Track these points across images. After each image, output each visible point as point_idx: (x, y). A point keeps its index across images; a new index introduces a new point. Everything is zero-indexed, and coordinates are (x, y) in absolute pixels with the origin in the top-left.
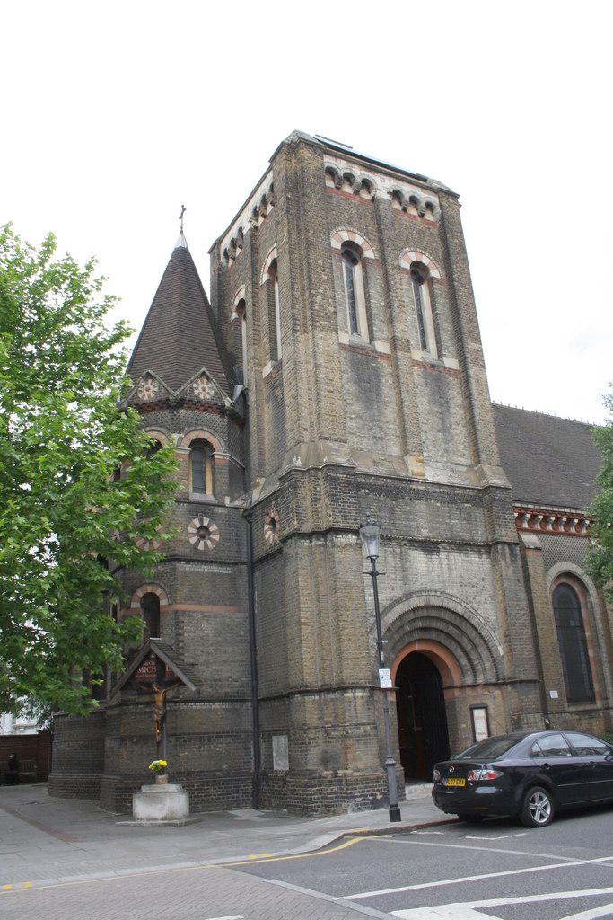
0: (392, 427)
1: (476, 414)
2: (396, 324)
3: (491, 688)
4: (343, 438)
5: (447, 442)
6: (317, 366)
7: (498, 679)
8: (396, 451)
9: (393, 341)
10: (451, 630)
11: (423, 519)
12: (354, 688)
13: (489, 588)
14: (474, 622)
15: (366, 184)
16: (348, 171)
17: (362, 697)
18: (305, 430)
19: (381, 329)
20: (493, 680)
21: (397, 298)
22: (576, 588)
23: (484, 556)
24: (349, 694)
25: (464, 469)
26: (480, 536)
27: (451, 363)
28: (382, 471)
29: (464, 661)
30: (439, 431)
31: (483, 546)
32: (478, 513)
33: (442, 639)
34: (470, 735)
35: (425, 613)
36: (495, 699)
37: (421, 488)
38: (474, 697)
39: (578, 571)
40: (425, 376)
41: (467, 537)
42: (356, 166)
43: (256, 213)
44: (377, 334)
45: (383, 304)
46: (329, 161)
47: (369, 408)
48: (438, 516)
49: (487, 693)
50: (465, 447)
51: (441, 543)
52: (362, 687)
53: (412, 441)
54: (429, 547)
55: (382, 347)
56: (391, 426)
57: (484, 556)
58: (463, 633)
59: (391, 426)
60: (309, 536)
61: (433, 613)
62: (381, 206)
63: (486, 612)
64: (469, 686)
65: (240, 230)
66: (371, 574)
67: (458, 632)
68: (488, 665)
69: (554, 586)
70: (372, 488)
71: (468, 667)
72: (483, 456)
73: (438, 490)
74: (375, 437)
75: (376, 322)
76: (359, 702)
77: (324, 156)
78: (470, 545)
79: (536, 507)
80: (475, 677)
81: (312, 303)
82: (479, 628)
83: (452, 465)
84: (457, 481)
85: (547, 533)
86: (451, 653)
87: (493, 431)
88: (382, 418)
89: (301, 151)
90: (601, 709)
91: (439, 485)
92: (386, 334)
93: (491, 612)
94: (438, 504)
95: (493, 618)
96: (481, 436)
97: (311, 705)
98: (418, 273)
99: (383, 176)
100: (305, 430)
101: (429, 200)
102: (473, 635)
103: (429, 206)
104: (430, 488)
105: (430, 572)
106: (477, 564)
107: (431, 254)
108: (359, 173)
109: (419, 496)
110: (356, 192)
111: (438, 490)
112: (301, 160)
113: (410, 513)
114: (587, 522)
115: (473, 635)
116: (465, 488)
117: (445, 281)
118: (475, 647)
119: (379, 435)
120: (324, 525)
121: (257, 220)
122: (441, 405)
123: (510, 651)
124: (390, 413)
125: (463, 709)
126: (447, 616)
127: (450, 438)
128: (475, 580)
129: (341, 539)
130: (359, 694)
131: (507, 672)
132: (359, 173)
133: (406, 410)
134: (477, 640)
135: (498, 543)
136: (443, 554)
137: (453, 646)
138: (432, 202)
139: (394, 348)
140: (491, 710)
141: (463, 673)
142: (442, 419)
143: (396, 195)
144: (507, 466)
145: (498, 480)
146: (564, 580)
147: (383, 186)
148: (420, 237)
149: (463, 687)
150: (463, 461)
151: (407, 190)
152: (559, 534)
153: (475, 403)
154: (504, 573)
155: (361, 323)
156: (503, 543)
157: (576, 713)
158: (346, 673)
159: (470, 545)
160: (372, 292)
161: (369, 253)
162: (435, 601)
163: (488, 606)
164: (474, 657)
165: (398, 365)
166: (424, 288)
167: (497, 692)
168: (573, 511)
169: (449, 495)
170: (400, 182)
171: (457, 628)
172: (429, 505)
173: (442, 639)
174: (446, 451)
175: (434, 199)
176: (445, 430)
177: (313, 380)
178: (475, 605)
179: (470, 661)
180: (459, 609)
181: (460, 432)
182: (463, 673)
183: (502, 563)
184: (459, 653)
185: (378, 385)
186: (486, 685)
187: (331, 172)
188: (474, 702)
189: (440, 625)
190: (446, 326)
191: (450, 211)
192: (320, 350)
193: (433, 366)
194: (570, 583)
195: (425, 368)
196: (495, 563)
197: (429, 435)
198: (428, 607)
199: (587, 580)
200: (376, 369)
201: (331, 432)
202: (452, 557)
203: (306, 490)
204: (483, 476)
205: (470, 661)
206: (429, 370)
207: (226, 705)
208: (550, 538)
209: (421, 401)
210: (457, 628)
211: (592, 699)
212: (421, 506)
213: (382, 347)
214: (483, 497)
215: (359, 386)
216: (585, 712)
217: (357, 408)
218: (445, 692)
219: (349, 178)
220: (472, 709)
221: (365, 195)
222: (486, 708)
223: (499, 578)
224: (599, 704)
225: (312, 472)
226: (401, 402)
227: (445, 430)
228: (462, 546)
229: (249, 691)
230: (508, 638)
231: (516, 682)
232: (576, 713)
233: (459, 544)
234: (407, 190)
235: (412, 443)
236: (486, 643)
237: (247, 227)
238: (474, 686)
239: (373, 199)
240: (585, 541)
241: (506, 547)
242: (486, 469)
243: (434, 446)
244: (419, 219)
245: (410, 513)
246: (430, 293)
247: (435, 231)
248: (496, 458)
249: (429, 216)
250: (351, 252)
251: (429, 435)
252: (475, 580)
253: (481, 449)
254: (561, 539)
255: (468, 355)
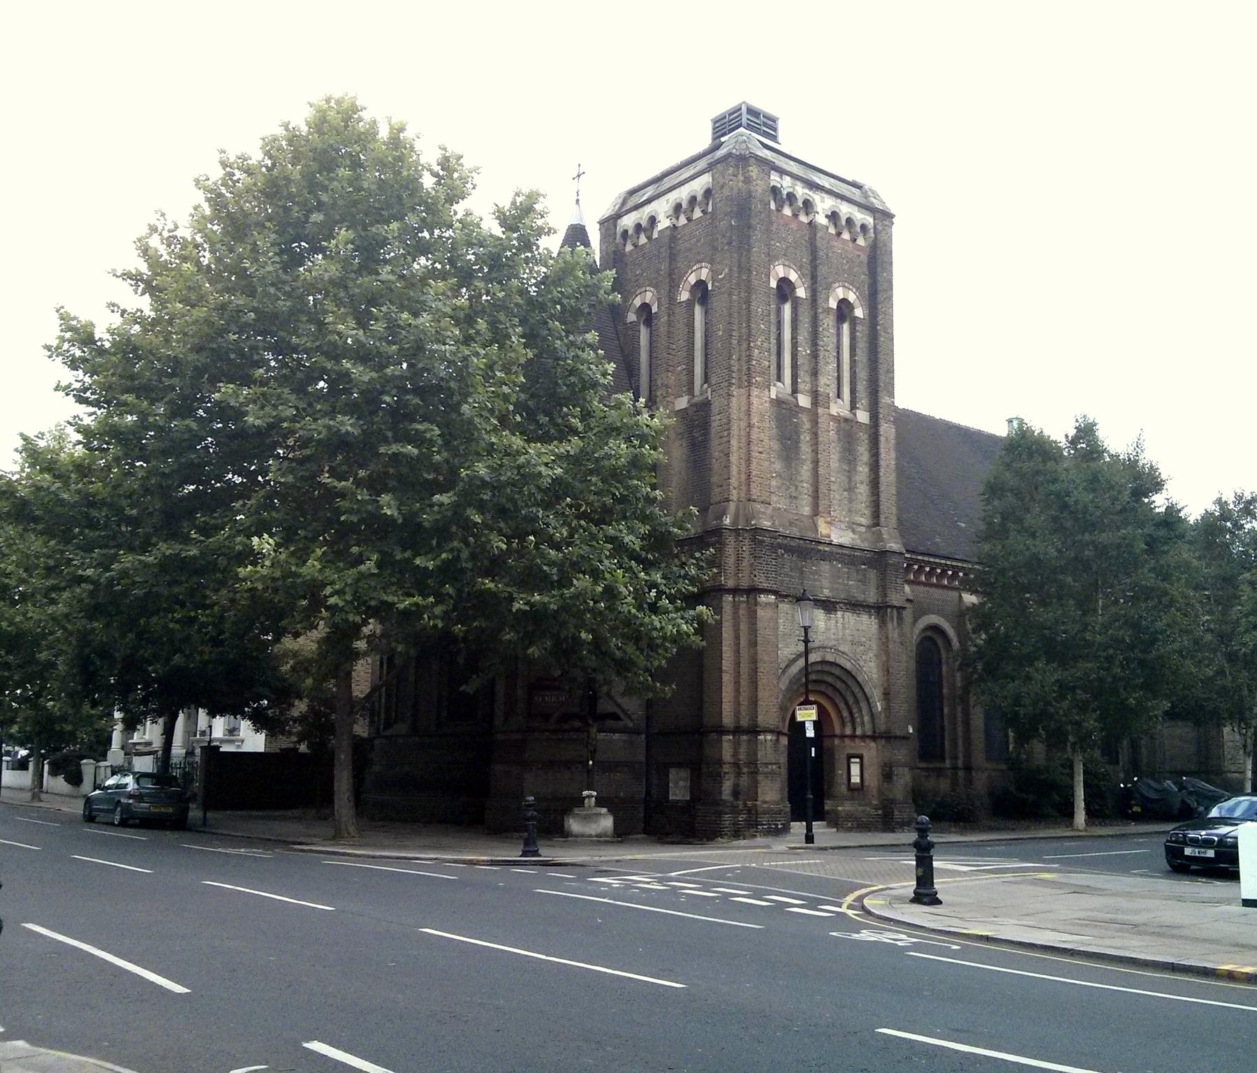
0: (806, 486)
1: (881, 474)
2: (820, 377)
3: (868, 741)
4: (768, 500)
5: (851, 501)
6: (750, 426)
7: (874, 732)
8: (807, 510)
9: (815, 395)
10: (839, 685)
11: (825, 579)
12: (765, 731)
13: (874, 647)
14: (859, 679)
15: (808, 205)
16: (791, 190)
17: (771, 740)
18: (734, 488)
19: (805, 382)
20: (869, 733)
21: (823, 347)
22: (940, 642)
23: (873, 617)
24: (761, 737)
25: (863, 529)
26: (872, 597)
27: (863, 416)
28: (795, 532)
29: (845, 714)
30: (845, 490)
31: (873, 607)
32: (873, 575)
33: (830, 692)
34: (845, 781)
35: (819, 668)
36: (871, 751)
37: (827, 549)
38: (852, 748)
39: (946, 626)
40: (838, 432)
41: (861, 597)
42: (799, 183)
43: (678, 208)
44: (801, 386)
45: (808, 352)
46: (775, 178)
47: (788, 467)
48: (839, 578)
49: (863, 744)
50: (867, 507)
51: (838, 603)
52: (771, 732)
53: (823, 502)
54: (829, 606)
55: (804, 401)
56: (805, 485)
57: (873, 617)
58: (848, 686)
59: (805, 485)
60: (735, 591)
61: (827, 668)
62: (819, 235)
63: (869, 670)
64: (847, 736)
65: (653, 220)
66: (804, 641)
67: (843, 686)
68: (866, 719)
69: (919, 639)
70: (789, 550)
71: (848, 719)
72: (882, 519)
73: (840, 551)
74: (791, 496)
75: (801, 373)
76: (769, 744)
77: (772, 172)
78: (862, 606)
79: (913, 557)
80: (854, 729)
81: (749, 358)
82: (863, 684)
83: (852, 526)
84: (859, 543)
85: (920, 583)
86: (836, 706)
87: (894, 492)
88: (798, 477)
89: (751, 168)
90: (948, 769)
91: (841, 546)
92: (808, 387)
93: (875, 671)
94: (840, 566)
95: (875, 676)
96: (883, 497)
97: (726, 744)
98: (785, 290)
99: (824, 195)
100: (734, 488)
101: (865, 222)
102: (857, 690)
103: (863, 227)
104: (834, 549)
105: (828, 629)
106: (866, 624)
107: (857, 289)
108: (801, 191)
109: (825, 557)
110: (795, 215)
111: (840, 551)
112: (747, 180)
113: (816, 573)
114: (961, 574)
115: (857, 690)
116: (864, 550)
117: (867, 322)
118: (857, 701)
119: (794, 494)
120: (745, 584)
121: (677, 218)
122: (849, 462)
123: (887, 709)
124: (805, 471)
125: (841, 758)
126: (837, 671)
127: (854, 497)
128: (864, 639)
129: (763, 598)
130: (769, 737)
131: (882, 727)
132: (801, 191)
133: (821, 471)
134: (860, 695)
135: (889, 606)
136: (839, 614)
137: (838, 700)
138: (867, 223)
139: (815, 403)
140: (865, 760)
141: (843, 725)
142: (849, 478)
143: (833, 216)
144: (903, 528)
145: (894, 545)
146: (929, 633)
147: (823, 204)
148: (850, 268)
149: (843, 737)
150: (863, 521)
151: (845, 210)
152: (932, 585)
153: (882, 463)
154: (890, 635)
155: (786, 371)
156: (893, 607)
157: (926, 769)
158: (760, 718)
159: (862, 606)
160: (800, 338)
161: (801, 292)
162: (830, 658)
163: (872, 664)
164: (855, 710)
165: (817, 423)
166: (846, 327)
167: (873, 744)
168: (948, 563)
169: (846, 555)
170: (839, 201)
171: (844, 682)
172: (832, 566)
173: (830, 692)
174: (850, 511)
175: (869, 220)
176: (850, 489)
177: (744, 440)
178: (862, 663)
179: (851, 713)
180: (848, 666)
181: (863, 490)
182: (843, 725)
183: (890, 626)
184: (842, 706)
185: (798, 442)
186: (864, 737)
187: (775, 191)
188: (852, 752)
189: (830, 679)
190: (863, 374)
191: (883, 237)
192: (754, 408)
193: (846, 420)
194: (935, 636)
195: (839, 423)
196: (882, 624)
197: (837, 495)
198: (823, 662)
199: (951, 633)
200: (797, 425)
201: (759, 494)
202: (846, 616)
203: (730, 540)
204: (879, 538)
205: (851, 713)
206: (843, 425)
207: (624, 737)
208: (921, 588)
209: (832, 459)
210: (844, 682)
211: (943, 759)
212: (825, 567)
213: (804, 401)
214: (878, 559)
215: (781, 443)
216: (934, 769)
217: (778, 466)
218: (824, 739)
219: (791, 197)
220: (850, 757)
221: (803, 219)
222: (861, 757)
223: (884, 641)
224: (948, 763)
225: (737, 532)
226: (816, 462)
227: (850, 489)
228: (855, 606)
229: (643, 725)
230: (886, 695)
231: (890, 737)
232: (926, 769)
233: (854, 605)
234: (845, 210)
235: (823, 504)
236: (868, 700)
237: (664, 223)
238: (853, 737)
239: (810, 223)
240: (955, 594)
241: (895, 612)
242: (884, 530)
243: (840, 506)
244: (851, 245)
245: (816, 573)
246: (851, 334)
247: (864, 258)
248: (893, 521)
249: (861, 242)
250: (785, 290)
251: (837, 495)
252: (864, 639)
253: (881, 511)
254: (932, 590)
255: (881, 411)
